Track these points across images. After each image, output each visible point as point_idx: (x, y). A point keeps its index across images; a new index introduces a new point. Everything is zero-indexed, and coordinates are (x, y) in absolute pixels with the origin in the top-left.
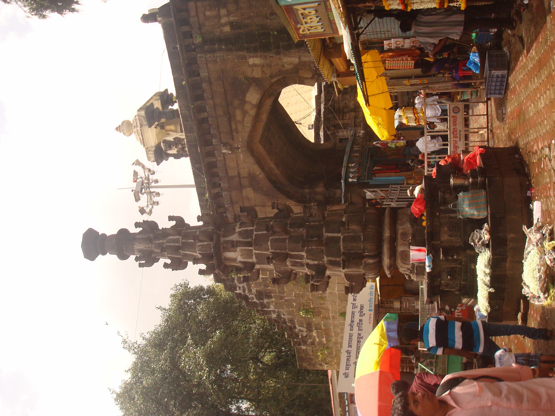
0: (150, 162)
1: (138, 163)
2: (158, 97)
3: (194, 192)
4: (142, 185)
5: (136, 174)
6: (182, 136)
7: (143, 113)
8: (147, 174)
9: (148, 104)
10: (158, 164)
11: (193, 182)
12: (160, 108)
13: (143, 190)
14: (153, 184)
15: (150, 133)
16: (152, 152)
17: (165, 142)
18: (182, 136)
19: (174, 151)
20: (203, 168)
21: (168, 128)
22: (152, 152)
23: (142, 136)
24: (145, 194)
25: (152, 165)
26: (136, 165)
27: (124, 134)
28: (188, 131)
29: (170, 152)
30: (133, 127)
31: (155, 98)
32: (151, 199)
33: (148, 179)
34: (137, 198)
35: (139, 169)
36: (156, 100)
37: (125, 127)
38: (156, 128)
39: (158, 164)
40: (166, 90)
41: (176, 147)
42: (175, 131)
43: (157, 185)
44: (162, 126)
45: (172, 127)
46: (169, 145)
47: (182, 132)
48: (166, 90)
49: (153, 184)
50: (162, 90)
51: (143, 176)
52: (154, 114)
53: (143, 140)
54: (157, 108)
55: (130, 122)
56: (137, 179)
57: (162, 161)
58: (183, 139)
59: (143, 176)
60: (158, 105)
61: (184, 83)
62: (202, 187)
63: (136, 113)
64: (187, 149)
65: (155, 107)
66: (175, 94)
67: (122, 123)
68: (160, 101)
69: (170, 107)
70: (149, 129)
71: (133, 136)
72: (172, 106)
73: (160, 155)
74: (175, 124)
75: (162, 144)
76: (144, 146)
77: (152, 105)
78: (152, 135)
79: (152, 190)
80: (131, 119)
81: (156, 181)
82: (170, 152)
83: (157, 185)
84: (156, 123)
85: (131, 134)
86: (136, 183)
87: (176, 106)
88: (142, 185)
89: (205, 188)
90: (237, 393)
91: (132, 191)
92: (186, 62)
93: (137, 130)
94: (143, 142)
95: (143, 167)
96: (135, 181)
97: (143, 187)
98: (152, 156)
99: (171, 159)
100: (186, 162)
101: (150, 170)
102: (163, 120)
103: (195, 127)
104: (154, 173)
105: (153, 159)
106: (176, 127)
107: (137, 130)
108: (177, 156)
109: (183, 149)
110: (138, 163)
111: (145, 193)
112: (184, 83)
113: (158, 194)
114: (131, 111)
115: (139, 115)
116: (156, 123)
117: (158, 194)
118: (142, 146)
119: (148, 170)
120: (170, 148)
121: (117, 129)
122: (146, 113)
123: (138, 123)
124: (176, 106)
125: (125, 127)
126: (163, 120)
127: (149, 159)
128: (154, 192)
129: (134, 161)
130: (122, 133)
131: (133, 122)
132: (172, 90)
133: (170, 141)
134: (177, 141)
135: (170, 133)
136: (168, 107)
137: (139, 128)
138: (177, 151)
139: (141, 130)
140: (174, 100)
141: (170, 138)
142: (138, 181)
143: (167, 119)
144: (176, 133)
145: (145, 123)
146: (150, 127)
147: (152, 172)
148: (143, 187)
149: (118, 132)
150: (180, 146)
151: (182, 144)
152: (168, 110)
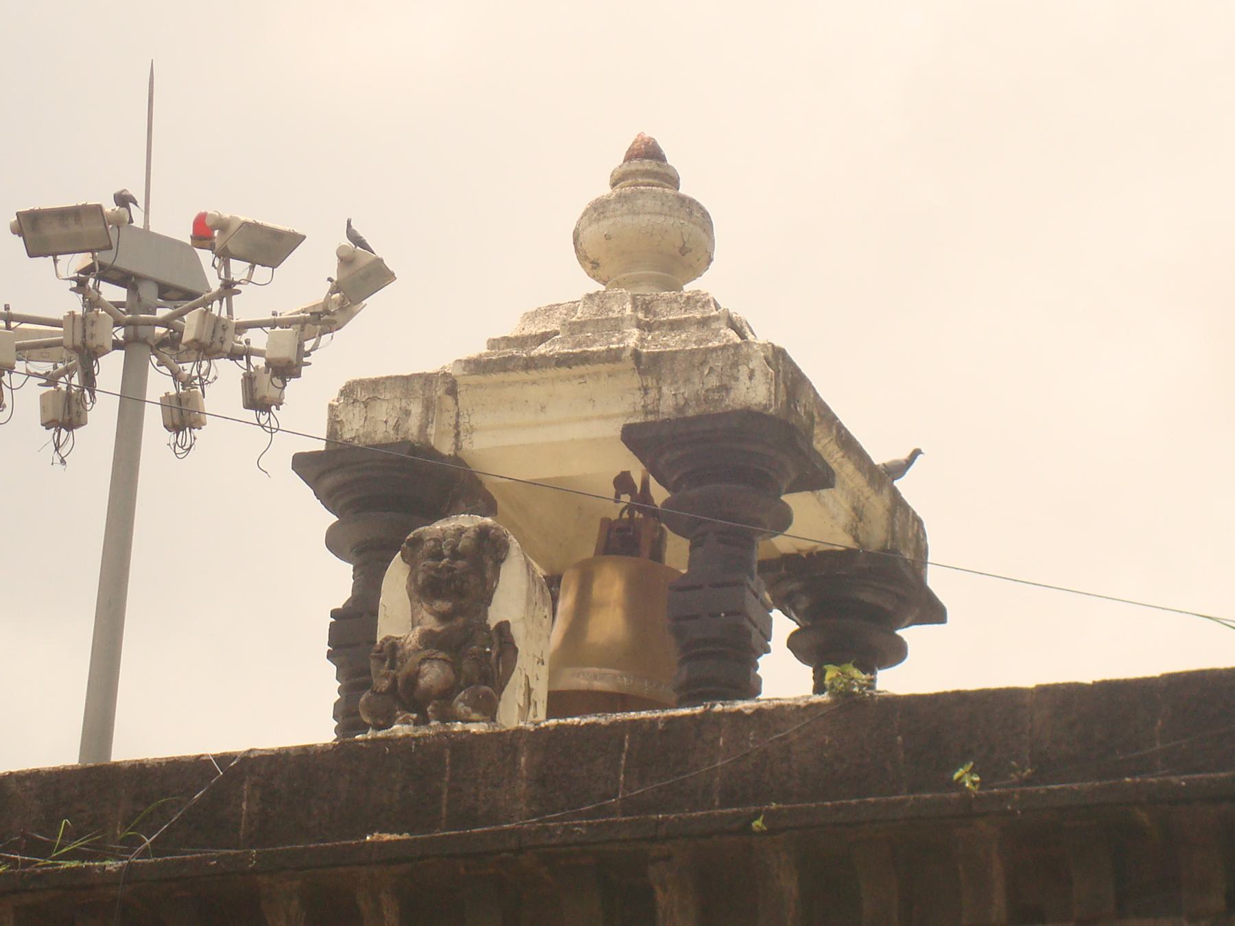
0: (333, 395)
1: (361, 276)
2: (877, 535)
3: (929, 560)
4: (166, 292)
5: (270, 246)
6: (522, 707)
7: (754, 391)
8: (257, 339)
9: (823, 444)
10: (305, 465)
11: (139, 740)
12: (783, 544)
13: (113, 293)
14: (159, 383)
15: (577, 432)
16: (413, 426)
17: (489, 550)
18: (522, 707)
19: (399, 616)
20: (214, 856)
21: (611, 586)
22: (413, 425)
23: (563, 361)
24: (76, 304)
25: (306, 416)
26: (346, 261)
27: (598, 209)
28: (558, 757)
29: (396, 576)
30: (648, 292)
31: (878, 506)
32: (26, 351)
33: (206, 349)
34: (52, 230)
35: (302, 282)
36: (858, 513)
37: (650, 224)
38: (623, 482)
39: (305, 465)
40: (933, 612)
41: (429, 639)
42: (574, 647)
43: (153, 417)
44: (625, 539)
45: (609, 625)
46: (458, 584)
47: (559, 702)
48: (933, 612)
49: (159, 383)
50: (936, 581)
51: (245, 307)
52: (743, 489)
53: (530, 364)
54: (783, 520)
55: (696, 271)
56: (225, 255)
57: (328, 499)
58: (488, 709)
59: (245, 307)
60: (815, 521)
61: (965, 776)
62: (50, 825)
63: (764, 333)
64: (400, 729)
65: (799, 503)
66: (892, 681)
67: (690, 207)
68: (843, 541)
69: (782, 626)
70: (614, 430)
71: (576, 285)
72: (794, 643)
73: (386, 489)
74: (634, 654)
75: (467, 521)
76: (478, 366)
77: (818, 478)
78: (565, 445)
79: (110, 368)
80: (716, 284)
81: (183, 416)
82: (396, 576)
83: (153, 417)
84: (659, 494)
85: (592, 265)
86: (184, 234)
87: (784, 677)
88: (166, 292)
89: (44, 850)
90: (122, 842)
91: (123, 200)
92: (1143, 817)
93: (616, 325)
94: (507, 362)
95: (322, 320)
96: (203, 231)
97: (148, 292)
98: (378, 425)
99: (337, 581)
100: (295, 708)
101: (285, 370)
102: (678, 552)
103: (580, 827)
104: (258, 401)
105: (354, 427)
106: (606, 657)
107: (616, 325)
108: (351, 634)
109: (408, 697)
110: (361, 276)
111: (92, 303)
112: (965, 776)
113: (66, 416)
114: (774, 289)
115: (736, 355)
116: (659, 494)
117: (66, 416)
118: (478, 348)
119: (286, 352)
120: (426, 589)
121: (647, 153)
122: (750, 416)
123: (672, 342)
124: (784, 677)
125: (650, 224)
126: (678, 552)
127: (360, 393)
128: (89, 381)
129: (382, 249)
130: (604, 190)
131: (692, 301)
132: (926, 665)
133: (486, 598)
134: (479, 657)
135: (566, 602)
136: (787, 605)
137: (632, 338)
138: (393, 646)
139: (613, 356)
140: (831, 673)
141: (511, 600)
142: (206, 257)
143: (682, 586)
144: (550, 645)
145: (670, 398)
146: (633, 437)
147: (265, 387)
148: (148, 292)
149: (615, 159)
150: (432, 675)
151: (446, 695)
152: (752, 606)
